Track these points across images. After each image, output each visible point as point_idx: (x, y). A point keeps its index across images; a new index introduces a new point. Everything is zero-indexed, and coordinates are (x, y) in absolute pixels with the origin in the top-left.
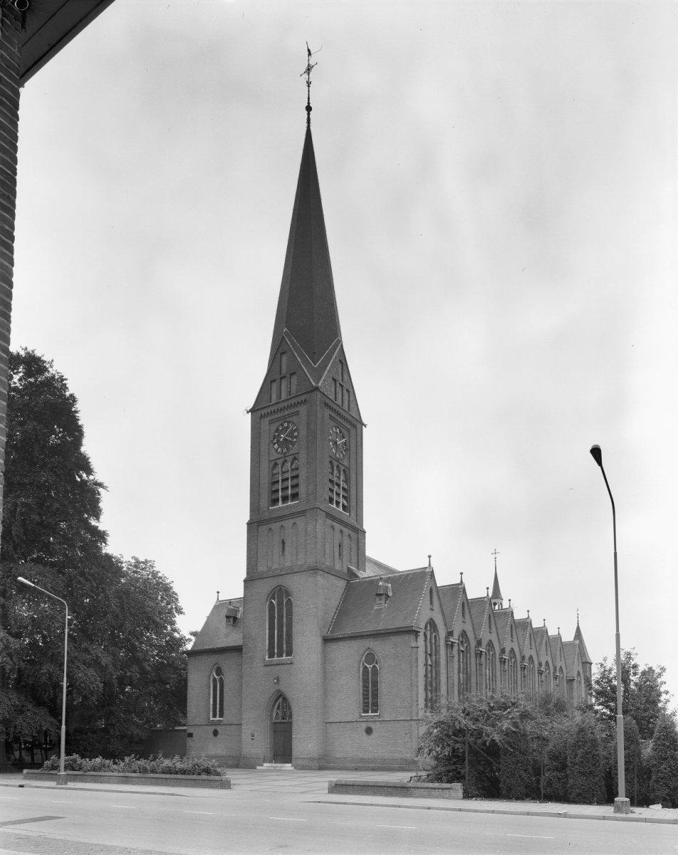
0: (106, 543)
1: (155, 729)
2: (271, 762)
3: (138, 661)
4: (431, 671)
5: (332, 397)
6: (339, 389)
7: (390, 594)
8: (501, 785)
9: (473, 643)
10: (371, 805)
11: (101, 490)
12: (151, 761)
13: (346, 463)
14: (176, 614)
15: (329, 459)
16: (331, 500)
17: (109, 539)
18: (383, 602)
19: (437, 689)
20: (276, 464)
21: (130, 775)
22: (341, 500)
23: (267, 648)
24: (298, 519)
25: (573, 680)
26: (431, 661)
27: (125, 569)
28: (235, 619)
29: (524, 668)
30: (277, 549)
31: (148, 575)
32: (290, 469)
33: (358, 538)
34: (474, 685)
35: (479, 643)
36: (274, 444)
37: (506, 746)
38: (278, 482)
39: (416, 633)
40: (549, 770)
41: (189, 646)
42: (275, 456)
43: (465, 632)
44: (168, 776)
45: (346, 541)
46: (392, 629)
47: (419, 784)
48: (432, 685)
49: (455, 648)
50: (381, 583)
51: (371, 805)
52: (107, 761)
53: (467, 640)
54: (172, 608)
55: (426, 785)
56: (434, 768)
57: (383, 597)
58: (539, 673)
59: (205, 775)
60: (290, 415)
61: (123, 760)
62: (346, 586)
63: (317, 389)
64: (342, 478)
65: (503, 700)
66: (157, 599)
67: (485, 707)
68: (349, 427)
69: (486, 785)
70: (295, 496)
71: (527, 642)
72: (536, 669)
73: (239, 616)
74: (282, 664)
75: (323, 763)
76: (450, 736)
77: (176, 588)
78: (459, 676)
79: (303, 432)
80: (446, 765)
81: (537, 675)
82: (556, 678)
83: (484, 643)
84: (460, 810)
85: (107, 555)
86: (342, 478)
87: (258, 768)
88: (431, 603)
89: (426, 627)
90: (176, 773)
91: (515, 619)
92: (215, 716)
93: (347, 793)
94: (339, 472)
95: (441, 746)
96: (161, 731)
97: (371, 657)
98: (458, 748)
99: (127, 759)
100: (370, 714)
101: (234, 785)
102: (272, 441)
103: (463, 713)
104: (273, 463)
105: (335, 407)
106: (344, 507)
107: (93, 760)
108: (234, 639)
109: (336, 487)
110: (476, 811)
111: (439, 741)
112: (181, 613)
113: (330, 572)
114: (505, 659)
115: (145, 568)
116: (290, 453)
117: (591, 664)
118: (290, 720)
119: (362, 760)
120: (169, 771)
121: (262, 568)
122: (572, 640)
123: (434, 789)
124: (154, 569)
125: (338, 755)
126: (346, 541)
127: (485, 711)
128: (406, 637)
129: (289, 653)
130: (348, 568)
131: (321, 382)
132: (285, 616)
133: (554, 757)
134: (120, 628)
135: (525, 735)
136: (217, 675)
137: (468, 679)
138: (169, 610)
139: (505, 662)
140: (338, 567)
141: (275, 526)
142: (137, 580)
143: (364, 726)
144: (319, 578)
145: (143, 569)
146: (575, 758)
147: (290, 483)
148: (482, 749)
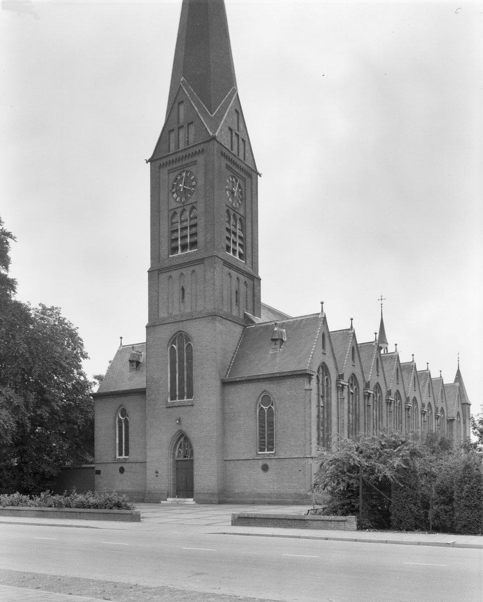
0: (14, 291)
1: (64, 466)
2: (174, 497)
3: (46, 402)
4: (323, 412)
5: (228, 147)
6: (235, 138)
7: (285, 339)
8: (392, 518)
9: (362, 386)
10: (273, 536)
11: (9, 240)
12: (65, 496)
13: (242, 212)
14: (81, 359)
15: (226, 208)
16: (228, 248)
17: (18, 288)
18: (278, 346)
19: (329, 429)
20: (175, 213)
21: (46, 509)
22: (238, 248)
23: (169, 391)
24: (198, 267)
25: (452, 420)
26: (323, 402)
27: (33, 316)
28: (138, 363)
29: (409, 409)
30: (177, 295)
31: (54, 322)
32: (188, 217)
33: (254, 285)
34: (362, 424)
35: (367, 385)
36: (173, 193)
37: (397, 482)
38: (177, 230)
39: (309, 376)
40: (437, 503)
41: (95, 389)
42: (174, 205)
43: (355, 375)
44: (81, 510)
45: (243, 288)
46: (287, 372)
47: (317, 517)
48: (324, 425)
49: (346, 391)
50: (276, 329)
51: (273, 536)
52: (25, 497)
53: (400, 398)
54: (77, 353)
55: (322, 517)
56: (330, 502)
57: (278, 342)
58: (422, 414)
59: (116, 508)
60: (187, 165)
61: (39, 495)
62: (243, 331)
63: (214, 138)
64: (238, 226)
65: (393, 439)
66: (63, 344)
67: (377, 446)
68: (244, 176)
69: (378, 517)
70: (194, 244)
71: (411, 384)
72: (384, 398)
73: (141, 360)
74: (183, 406)
75: (223, 497)
76: (345, 472)
77: (81, 334)
78: (349, 417)
79: (201, 182)
80: (341, 500)
81: (420, 415)
82: (437, 418)
83: (372, 386)
84: (356, 540)
85: (16, 302)
86: (238, 226)
87: (162, 502)
88: (324, 347)
89: (318, 371)
90: (89, 507)
91: (330, 330)
92: (121, 454)
93: (248, 525)
94: (236, 221)
95: (336, 482)
96: (69, 468)
97: (266, 399)
98: (353, 484)
99: (42, 495)
100: (266, 452)
101: (143, 518)
102: (171, 191)
103: (357, 451)
104: (172, 212)
105: (231, 156)
106: (241, 255)
107: (12, 495)
108: (138, 381)
109: (233, 235)
110: (370, 541)
111: (335, 477)
112: (86, 358)
113: (227, 318)
114: (391, 401)
115: (52, 315)
116: (189, 202)
117: (470, 405)
118: (191, 458)
119: (259, 495)
120: (82, 505)
121: (163, 314)
122: (453, 382)
123: (331, 521)
124: (60, 315)
125: (237, 491)
126: (243, 288)
127: (377, 450)
128: (301, 380)
129: (190, 395)
130: (245, 314)
131: (218, 131)
132: (185, 360)
133: (441, 492)
134: (30, 374)
135: (414, 472)
136: (122, 416)
137: (357, 420)
138: (75, 355)
139: (390, 403)
140: (235, 313)
141: (175, 274)
142: (44, 326)
143: (261, 463)
144: (218, 324)
145: (50, 316)
146: (461, 492)
147: (188, 232)
148: (375, 485)
